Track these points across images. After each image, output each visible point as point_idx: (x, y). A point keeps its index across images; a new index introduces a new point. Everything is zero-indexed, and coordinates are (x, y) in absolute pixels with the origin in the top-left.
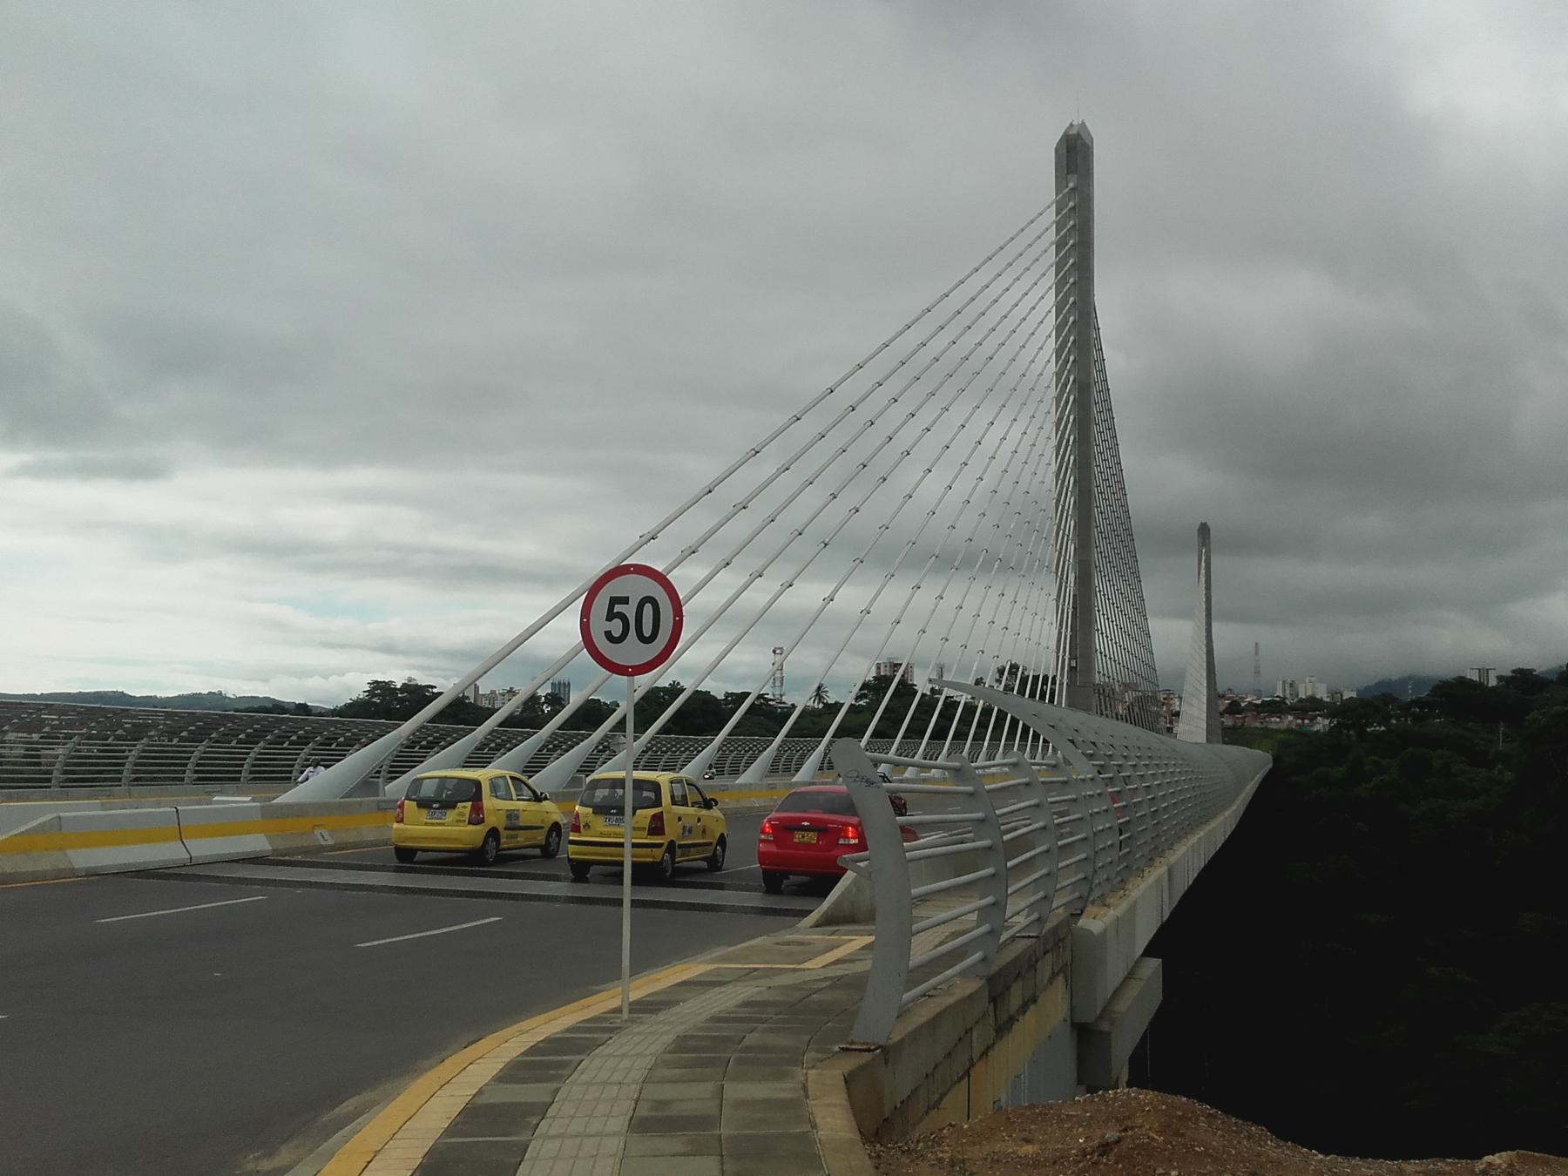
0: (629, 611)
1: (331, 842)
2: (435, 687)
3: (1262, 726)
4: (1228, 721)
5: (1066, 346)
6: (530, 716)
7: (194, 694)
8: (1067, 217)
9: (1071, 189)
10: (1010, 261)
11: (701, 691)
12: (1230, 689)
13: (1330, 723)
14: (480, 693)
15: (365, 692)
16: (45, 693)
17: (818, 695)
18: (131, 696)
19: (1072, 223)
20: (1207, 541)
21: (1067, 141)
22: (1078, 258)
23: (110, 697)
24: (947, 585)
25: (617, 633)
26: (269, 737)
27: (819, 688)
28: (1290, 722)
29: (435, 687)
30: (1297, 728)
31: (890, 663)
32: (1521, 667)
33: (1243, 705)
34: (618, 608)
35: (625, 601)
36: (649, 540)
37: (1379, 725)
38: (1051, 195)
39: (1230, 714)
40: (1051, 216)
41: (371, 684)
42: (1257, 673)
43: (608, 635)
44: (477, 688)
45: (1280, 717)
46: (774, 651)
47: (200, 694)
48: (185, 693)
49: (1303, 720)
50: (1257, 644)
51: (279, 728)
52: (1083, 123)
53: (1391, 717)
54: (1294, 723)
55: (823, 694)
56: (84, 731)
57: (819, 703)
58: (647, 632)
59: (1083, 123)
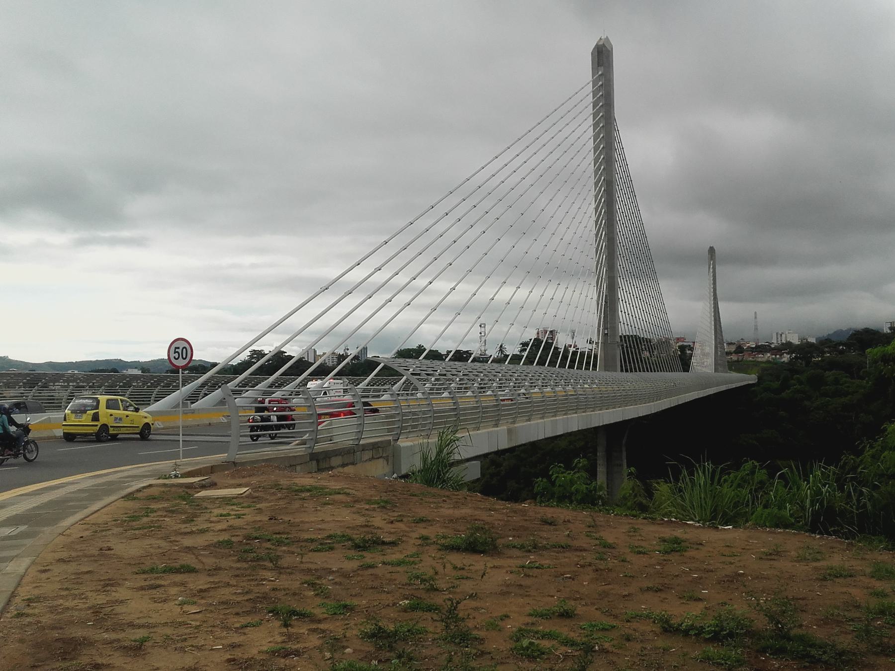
0: (180, 351)
1: (162, 426)
2: (286, 353)
3: (754, 360)
4: (734, 357)
5: (598, 161)
6: (268, 369)
7: (160, 359)
8: (598, 90)
9: (601, 75)
10: (555, 122)
11: (433, 350)
12: (742, 339)
13: (790, 357)
14: (317, 354)
15: (248, 356)
16: (78, 361)
17: (501, 350)
18: (125, 362)
19: (601, 93)
20: (713, 257)
21: (598, 48)
22: (605, 112)
23: (114, 362)
24: (546, 289)
25: (177, 357)
26: (162, 384)
27: (501, 346)
28: (769, 357)
29: (286, 353)
30: (773, 361)
31: (544, 330)
32: (868, 327)
33: (745, 348)
34: (177, 350)
35: (178, 348)
36: (325, 290)
37: (819, 356)
38: (591, 79)
39: (735, 353)
40: (590, 88)
41: (251, 352)
42: (756, 329)
43: (174, 357)
44: (315, 351)
45: (763, 355)
46: (480, 326)
47: (163, 359)
48: (155, 359)
49: (776, 355)
50: (756, 313)
51: (166, 380)
52: (607, 37)
53: (825, 352)
54: (771, 357)
55: (504, 350)
56: (75, 384)
57: (501, 354)
58: (184, 357)
59: (607, 37)
